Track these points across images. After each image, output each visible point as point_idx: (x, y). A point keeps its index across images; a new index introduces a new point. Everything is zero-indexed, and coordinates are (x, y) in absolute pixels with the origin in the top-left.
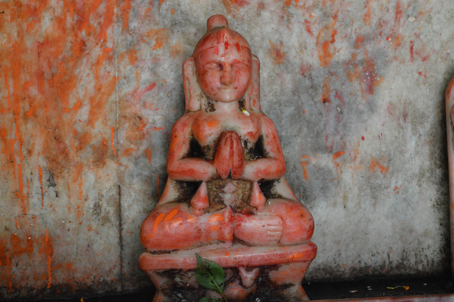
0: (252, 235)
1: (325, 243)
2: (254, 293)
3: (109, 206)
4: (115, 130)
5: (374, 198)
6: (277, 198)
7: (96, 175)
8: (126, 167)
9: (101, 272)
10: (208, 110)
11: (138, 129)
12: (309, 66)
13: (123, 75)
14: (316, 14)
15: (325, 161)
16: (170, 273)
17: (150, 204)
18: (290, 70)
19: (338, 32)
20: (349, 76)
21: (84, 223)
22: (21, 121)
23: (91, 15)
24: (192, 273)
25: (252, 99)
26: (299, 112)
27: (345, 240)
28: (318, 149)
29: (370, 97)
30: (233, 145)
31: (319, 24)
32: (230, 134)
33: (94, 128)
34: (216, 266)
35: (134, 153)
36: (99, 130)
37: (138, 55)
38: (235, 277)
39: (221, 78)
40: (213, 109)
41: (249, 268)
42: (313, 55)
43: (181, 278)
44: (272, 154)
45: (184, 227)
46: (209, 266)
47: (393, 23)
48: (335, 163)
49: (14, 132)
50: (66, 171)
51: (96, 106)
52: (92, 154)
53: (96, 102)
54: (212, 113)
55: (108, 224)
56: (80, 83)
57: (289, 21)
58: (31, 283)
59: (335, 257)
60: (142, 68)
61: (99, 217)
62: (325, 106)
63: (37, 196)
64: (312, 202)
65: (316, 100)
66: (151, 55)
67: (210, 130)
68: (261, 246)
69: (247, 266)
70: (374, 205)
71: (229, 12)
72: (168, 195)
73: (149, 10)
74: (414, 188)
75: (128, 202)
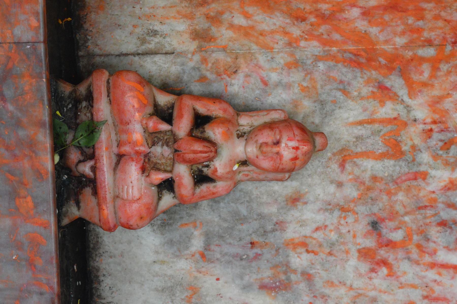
0: (124, 172)
1: (122, 243)
2: (72, 174)
3: (155, 44)
4: (224, 49)
5: (163, 290)
6: (159, 196)
7: (183, 32)
8: (191, 60)
9: (96, 37)
10: (238, 132)
11: (226, 70)
12: (285, 229)
13: (275, 56)
14: (333, 236)
15: (197, 244)
16: (90, 97)
17: (158, 81)
18: (281, 211)
19: (316, 256)
21: (140, 21)
23: (330, 27)
24: (90, 117)
25: (249, 173)
27: (124, 262)
29: (256, 286)
30: (204, 153)
31: (324, 239)
32: (213, 150)
33: (226, 29)
34: (96, 139)
35: (203, 67)
36: (224, 34)
37: (294, 70)
38: (87, 157)
39: (266, 144)
40: (239, 136)
41: (94, 169)
42: (294, 232)
43: (85, 107)
44: (198, 191)
45: (131, 109)
46: (96, 132)
48: (195, 253)
50: (187, 5)
51: (246, 32)
52: (202, 28)
53: (250, 32)
54: (235, 136)
55: (139, 43)
56: (267, 17)
57: (326, 210)
59: (109, 253)
60: (282, 74)
61: (145, 35)
62: (248, 244)
64: (159, 231)
66: (293, 82)
67: (219, 133)
68: (114, 181)
69: (95, 167)
70: (157, 290)
71: (334, 154)
72: (162, 96)
73: (335, 80)
75: (159, 61)
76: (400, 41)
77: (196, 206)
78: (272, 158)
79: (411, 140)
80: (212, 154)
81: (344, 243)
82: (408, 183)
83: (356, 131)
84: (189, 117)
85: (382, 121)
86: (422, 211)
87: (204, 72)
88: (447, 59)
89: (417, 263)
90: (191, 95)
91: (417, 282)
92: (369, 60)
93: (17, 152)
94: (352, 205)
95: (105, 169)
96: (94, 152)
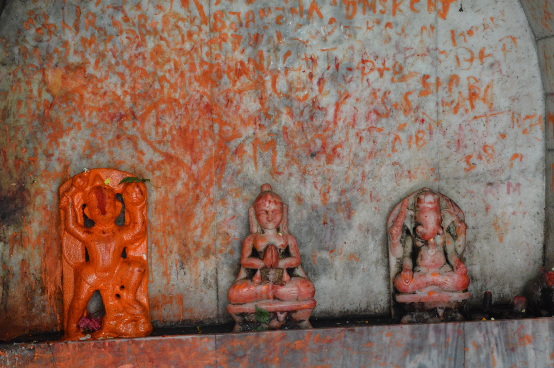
4: (214, 240)
8: (220, 259)
14: (320, 178)
15: (325, 255)
16: (242, 315)
17: (232, 278)
20: (337, 210)
22: (166, 236)
26: (311, 231)
28: (321, 249)
29: (349, 221)
35: (224, 252)
36: (206, 240)
37: (226, 201)
39: (267, 218)
40: (263, 232)
41: (282, 312)
44: (293, 255)
47: (360, 182)
49: (163, 241)
51: (205, 228)
57: (305, 182)
58: (172, 319)
63: (174, 274)
65: (320, 223)
70: (352, 278)
71: (273, 178)
73: (232, 178)
76: (210, 143)
77: (302, 256)
78: (275, 215)
79: (265, 136)
80: (273, 248)
81: (324, 173)
82: (289, 137)
83: (260, 166)
84: (253, 260)
85: (255, 152)
86: (305, 129)
87: (227, 251)
88: (220, 117)
89: (334, 131)
90: (240, 259)
91: (344, 131)
92: (220, 159)
93: (272, 349)
94: (302, 168)
95: (282, 306)
96: (273, 312)
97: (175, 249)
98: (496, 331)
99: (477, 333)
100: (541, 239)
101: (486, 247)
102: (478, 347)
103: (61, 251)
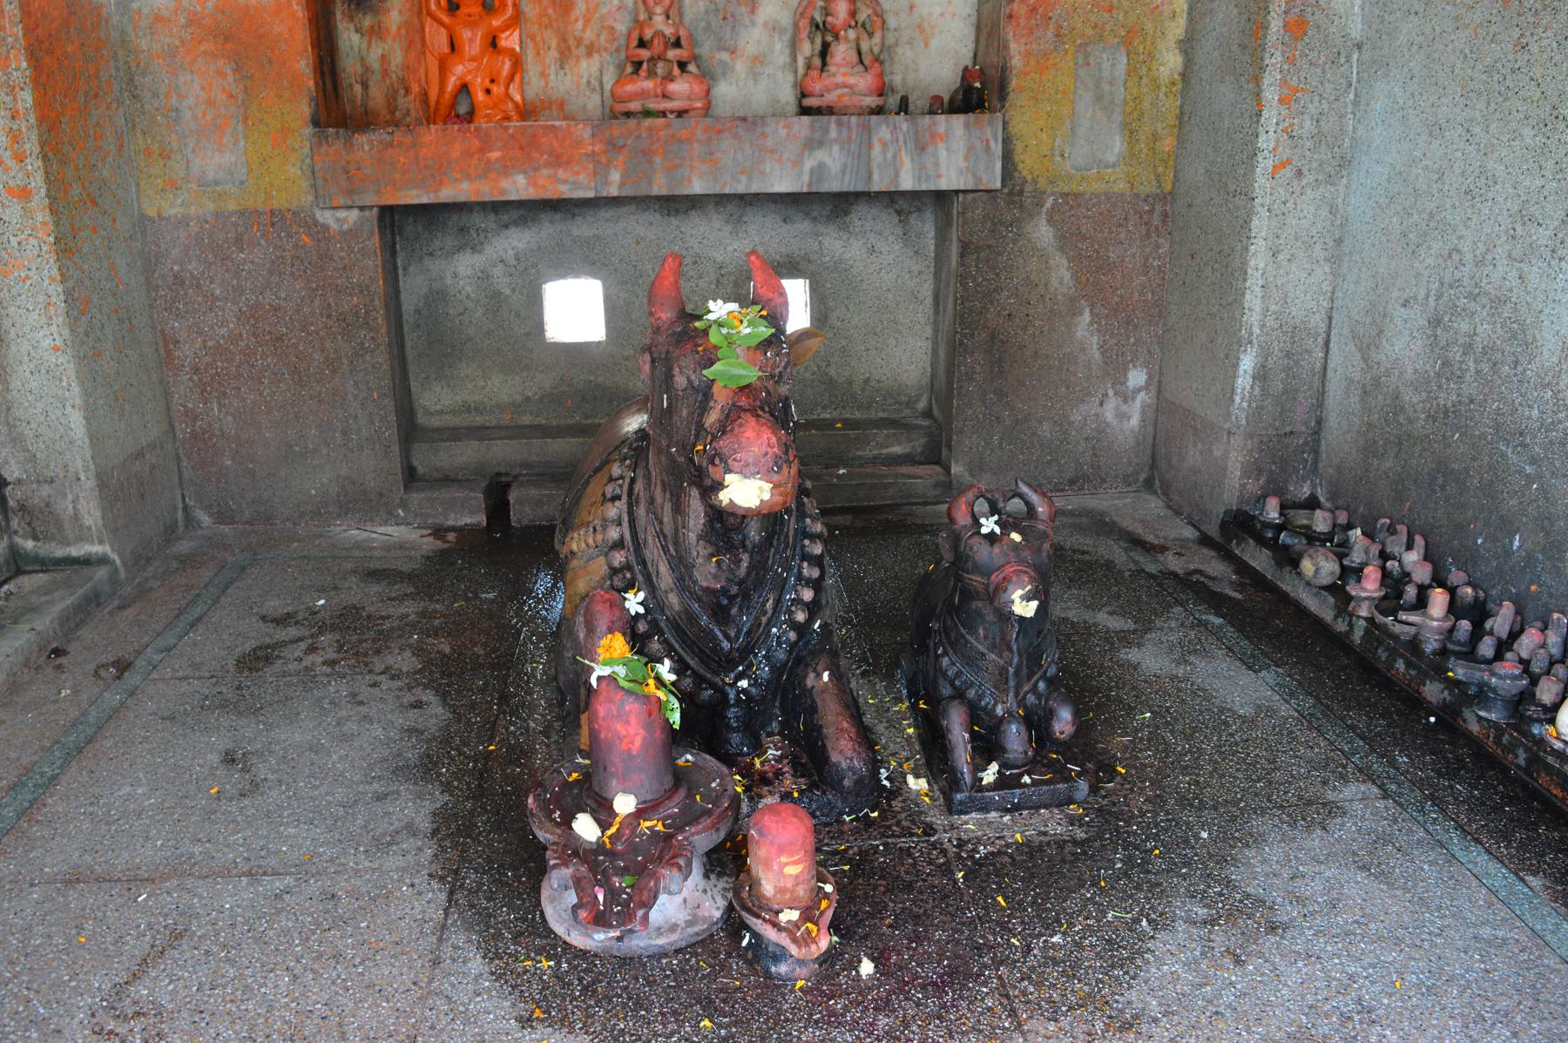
15: (725, 56)
28: (721, 49)
36: (589, 35)
51: (587, 21)
74: (779, 74)
97: (554, 45)
98: (905, 127)
99: (884, 128)
100: (971, 46)
101: (909, 54)
102: (884, 144)
103: (424, 41)
